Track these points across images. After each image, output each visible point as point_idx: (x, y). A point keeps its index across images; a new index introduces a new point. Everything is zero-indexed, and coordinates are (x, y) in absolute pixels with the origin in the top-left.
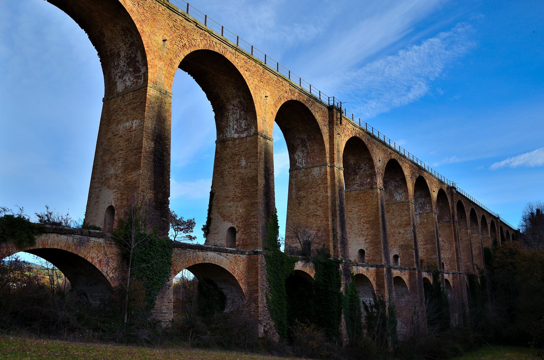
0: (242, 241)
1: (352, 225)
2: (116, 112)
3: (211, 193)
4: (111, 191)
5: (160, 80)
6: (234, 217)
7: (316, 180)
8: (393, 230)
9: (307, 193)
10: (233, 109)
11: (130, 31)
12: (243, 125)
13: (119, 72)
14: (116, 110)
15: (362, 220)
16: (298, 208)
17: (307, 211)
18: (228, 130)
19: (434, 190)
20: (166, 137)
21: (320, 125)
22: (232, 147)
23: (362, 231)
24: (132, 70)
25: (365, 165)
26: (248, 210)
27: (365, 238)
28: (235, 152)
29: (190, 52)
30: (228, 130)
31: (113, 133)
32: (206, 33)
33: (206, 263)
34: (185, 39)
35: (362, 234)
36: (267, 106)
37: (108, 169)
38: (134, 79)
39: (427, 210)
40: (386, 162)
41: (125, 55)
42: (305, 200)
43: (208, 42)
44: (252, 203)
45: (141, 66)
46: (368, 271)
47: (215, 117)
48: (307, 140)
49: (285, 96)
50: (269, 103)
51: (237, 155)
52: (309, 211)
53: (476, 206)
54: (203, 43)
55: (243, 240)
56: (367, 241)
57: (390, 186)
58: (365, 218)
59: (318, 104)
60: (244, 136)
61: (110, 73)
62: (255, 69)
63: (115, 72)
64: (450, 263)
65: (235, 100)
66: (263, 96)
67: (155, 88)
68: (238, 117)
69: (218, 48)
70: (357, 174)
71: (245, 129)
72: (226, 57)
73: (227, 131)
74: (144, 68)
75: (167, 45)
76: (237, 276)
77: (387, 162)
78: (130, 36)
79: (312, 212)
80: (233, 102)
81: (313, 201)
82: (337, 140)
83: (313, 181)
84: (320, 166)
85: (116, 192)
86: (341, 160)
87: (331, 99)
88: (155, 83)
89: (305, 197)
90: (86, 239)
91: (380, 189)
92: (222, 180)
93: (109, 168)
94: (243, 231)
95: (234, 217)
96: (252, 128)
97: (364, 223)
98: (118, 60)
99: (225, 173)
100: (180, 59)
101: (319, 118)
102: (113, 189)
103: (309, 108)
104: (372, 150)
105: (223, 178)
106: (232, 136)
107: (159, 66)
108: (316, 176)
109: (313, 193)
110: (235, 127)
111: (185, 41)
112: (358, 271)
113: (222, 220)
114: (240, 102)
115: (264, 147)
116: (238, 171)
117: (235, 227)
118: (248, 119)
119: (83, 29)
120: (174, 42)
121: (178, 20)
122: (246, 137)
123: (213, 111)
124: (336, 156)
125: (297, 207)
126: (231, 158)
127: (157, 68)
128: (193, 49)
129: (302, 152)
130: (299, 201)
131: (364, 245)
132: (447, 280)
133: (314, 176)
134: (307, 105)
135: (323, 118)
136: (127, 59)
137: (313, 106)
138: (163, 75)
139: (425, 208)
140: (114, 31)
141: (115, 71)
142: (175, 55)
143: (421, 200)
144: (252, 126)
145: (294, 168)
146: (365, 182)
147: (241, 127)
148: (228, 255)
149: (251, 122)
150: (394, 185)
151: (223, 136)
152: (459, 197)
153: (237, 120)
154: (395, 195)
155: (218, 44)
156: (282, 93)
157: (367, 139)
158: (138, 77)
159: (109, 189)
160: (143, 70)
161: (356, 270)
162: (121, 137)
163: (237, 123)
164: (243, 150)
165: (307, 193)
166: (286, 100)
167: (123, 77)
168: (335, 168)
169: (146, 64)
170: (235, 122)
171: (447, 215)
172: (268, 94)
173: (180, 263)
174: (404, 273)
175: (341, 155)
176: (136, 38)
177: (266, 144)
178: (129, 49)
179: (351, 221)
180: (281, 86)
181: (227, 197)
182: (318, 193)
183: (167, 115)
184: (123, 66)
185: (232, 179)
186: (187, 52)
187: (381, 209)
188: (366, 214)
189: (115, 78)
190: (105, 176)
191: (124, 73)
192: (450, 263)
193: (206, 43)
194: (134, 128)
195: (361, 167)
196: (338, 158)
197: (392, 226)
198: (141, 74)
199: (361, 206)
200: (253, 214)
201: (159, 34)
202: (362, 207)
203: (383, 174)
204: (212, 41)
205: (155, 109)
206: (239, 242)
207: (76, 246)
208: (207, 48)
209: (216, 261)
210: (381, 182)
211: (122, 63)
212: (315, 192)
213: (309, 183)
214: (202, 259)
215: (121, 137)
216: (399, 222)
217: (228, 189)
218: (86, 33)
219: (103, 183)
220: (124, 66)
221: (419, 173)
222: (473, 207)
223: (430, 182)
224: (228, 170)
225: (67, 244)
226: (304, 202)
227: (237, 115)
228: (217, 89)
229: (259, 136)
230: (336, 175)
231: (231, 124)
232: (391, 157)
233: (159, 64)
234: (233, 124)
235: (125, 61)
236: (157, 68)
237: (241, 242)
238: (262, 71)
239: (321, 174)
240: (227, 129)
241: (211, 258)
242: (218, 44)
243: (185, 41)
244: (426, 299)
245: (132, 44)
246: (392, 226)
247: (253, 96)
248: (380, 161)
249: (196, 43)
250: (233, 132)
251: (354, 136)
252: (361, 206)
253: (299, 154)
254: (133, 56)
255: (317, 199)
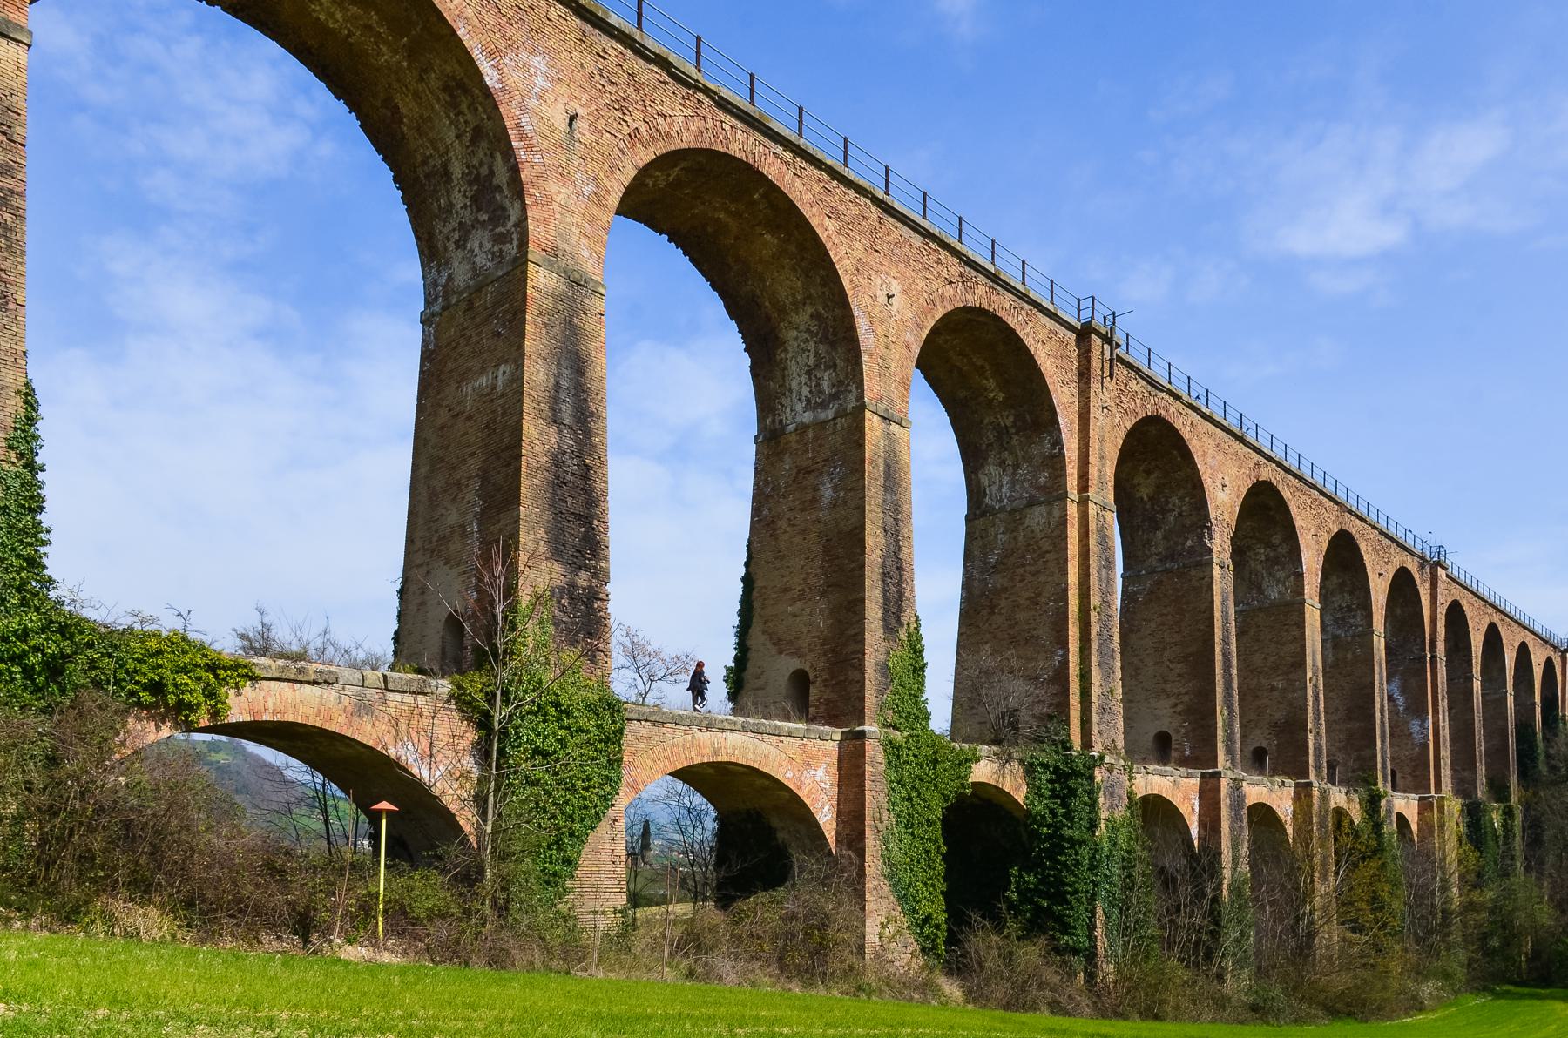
0: (826, 705)
1: (1139, 669)
2: (455, 347)
3: (744, 579)
4: (454, 572)
5: (567, 241)
6: (804, 643)
7: (1037, 542)
8: (1255, 681)
9: (1012, 579)
10: (796, 339)
11: (466, 91)
12: (825, 385)
13: (454, 230)
14: (454, 344)
15: (1166, 654)
16: (988, 620)
17: (1011, 627)
18: (787, 402)
19: (1382, 572)
20: (593, 412)
21: (1048, 381)
22: (796, 449)
23: (1166, 682)
24: (485, 217)
25: (1182, 499)
26: (840, 621)
27: (1173, 700)
28: (805, 464)
29: (654, 157)
30: (787, 402)
31: (450, 411)
32: (700, 96)
33: (721, 762)
34: (636, 114)
35: (1164, 691)
36: (893, 324)
37: (443, 511)
38: (493, 246)
39: (1356, 627)
40: (1244, 491)
41: (463, 173)
42: (1006, 599)
43: (710, 124)
44: (849, 602)
45: (507, 203)
46: (1178, 788)
47: (752, 368)
48: (1013, 431)
49: (947, 295)
50: (898, 317)
51: (809, 473)
52: (1017, 628)
53: (1504, 617)
54: (692, 128)
55: (828, 701)
56: (1179, 708)
57: (1252, 562)
58: (1174, 649)
59: (1045, 320)
60: (827, 416)
61: (431, 235)
62: (854, 211)
63: (445, 231)
64: (1414, 771)
65: (801, 313)
66: (879, 293)
67: (551, 266)
68: (811, 363)
69: (741, 144)
70: (1157, 528)
71: (830, 395)
72: (765, 173)
73: (782, 406)
74: (517, 205)
75: (580, 133)
76: (808, 797)
77: (1246, 489)
78: (469, 108)
79: (1024, 631)
80: (794, 318)
81: (1027, 599)
82: (1098, 424)
83: (1029, 545)
84: (1049, 503)
85: (464, 573)
86: (1109, 484)
87: (1086, 304)
88: (553, 251)
89: (1005, 589)
90: (377, 697)
91: (1222, 567)
92: (773, 543)
93: (445, 508)
94: (826, 680)
95: (804, 643)
96: (850, 391)
97: (1171, 662)
98: (448, 192)
99: (780, 523)
100: (622, 179)
101: (1048, 363)
102: (458, 565)
103: (1018, 331)
104: (1204, 455)
105: (776, 539)
106: (798, 419)
107: (560, 198)
108: (1037, 529)
109: (1029, 578)
110: (805, 391)
111: (636, 121)
112: (1149, 788)
113: (774, 650)
114: (816, 316)
115: (882, 443)
116: (814, 517)
117: (807, 668)
118: (838, 368)
119: (342, 101)
120: (601, 124)
121: (613, 52)
122: (834, 419)
123: (745, 350)
124: (1093, 472)
125: (985, 619)
126: (794, 481)
127: (555, 206)
128: (661, 148)
129: (1000, 466)
130: (991, 601)
131: (1170, 720)
132: (1400, 817)
133: (1032, 532)
134: (1012, 323)
135: (1059, 362)
136: (470, 183)
137: (1030, 325)
138: (573, 229)
139: (1352, 621)
140: (423, 96)
141: (444, 226)
142: (606, 167)
143: (1339, 600)
144: (848, 384)
145: (978, 512)
146: (1180, 547)
147: (821, 392)
148: (782, 742)
149: (847, 373)
150: (1263, 558)
151: (773, 421)
152: (1454, 591)
153: (809, 373)
154: (1264, 586)
155: (739, 132)
156: (936, 285)
157: (1189, 423)
158: (501, 239)
159: (447, 567)
160: (514, 215)
161: (1143, 783)
162: (469, 418)
163: (810, 379)
164: (825, 457)
165: (1012, 579)
166: (950, 308)
167: (466, 241)
168: (1091, 505)
169: (519, 193)
170: (804, 379)
171: (1415, 640)
172: (896, 288)
173: (649, 762)
174: (1279, 794)
175: (1110, 471)
176: (485, 112)
177: (889, 436)
178: (473, 151)
179: (1137, 656)
180: (935, 265)
181: (787, 590)
182: (1042, 579)
183: (592, 347)
184: (461, 208)
185: (798, 539)
186: (645, 156)
187: (1220, 621)
188: (1178, 638)
189: (446, 249)
190: (436, 532)
191: (465, 231)
192: (1414, 771)
193: (703, 130)
194: (499, 388)
195: (1170, 506)
196: (1100, 477)
197: (1251, 671)
198: (510, 224)
199: (1166, 615)
200: (853, 632)
201: (553, 98)
202: (1170, 617)
203: (1234, 524)
204: (722, 122)
205: (555, 330)
206: (817, 707)
207: (349, 715)
208: (706, 143)
209: (751, 756)
210: (1227, 545)
211: (458, 200)
212: (1033, 575)
213: (1018, 550)
214: (709, 751)
215: (469, 418)
216: (1272, 659)
217: (788, 567)
218: (350, 112)
219: (433, 551)
220: (465, 207)
221: (1341, 523)
222: (1496, 618)
223: (1370, 548)
224: (790, 515)
225: (322, 710)
226: (1003, 603)
227: (808, 357)
228: (750, 283)
229: (868, 414)
230: (1092, 526)
231: (794, 385)
232: (1257, 477)
233: (560, 192)
234: (800, 384)
235: (465, 191)
236: (555, 206)
237: (822, 708)
238: (876, 219)
239: (1050, 524)
240: (783, 400)
241: (734, 750)
242: (739, 132)
243: (636, 121)
244: (1337, 864)
245: (478, 134)
246: (1251, 671)
247: (849, 293)
248: (1224, 486)
249: (671, 126)
250: (799, 407)
251: (1149, 414)
252: (1166, 615)
253: (991, 473)
254: (484, 171)
255: (1039, 595)
